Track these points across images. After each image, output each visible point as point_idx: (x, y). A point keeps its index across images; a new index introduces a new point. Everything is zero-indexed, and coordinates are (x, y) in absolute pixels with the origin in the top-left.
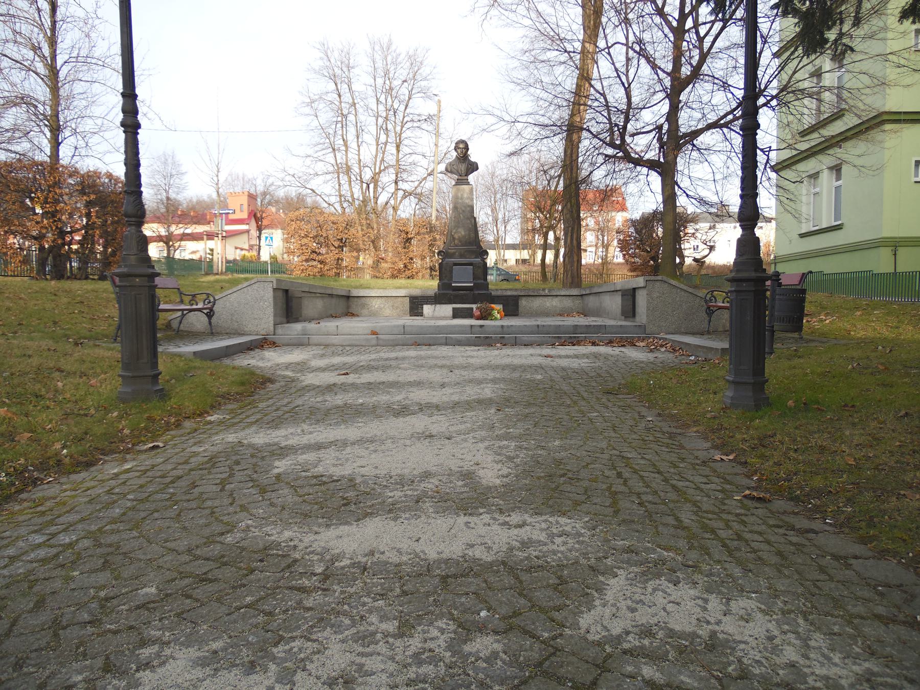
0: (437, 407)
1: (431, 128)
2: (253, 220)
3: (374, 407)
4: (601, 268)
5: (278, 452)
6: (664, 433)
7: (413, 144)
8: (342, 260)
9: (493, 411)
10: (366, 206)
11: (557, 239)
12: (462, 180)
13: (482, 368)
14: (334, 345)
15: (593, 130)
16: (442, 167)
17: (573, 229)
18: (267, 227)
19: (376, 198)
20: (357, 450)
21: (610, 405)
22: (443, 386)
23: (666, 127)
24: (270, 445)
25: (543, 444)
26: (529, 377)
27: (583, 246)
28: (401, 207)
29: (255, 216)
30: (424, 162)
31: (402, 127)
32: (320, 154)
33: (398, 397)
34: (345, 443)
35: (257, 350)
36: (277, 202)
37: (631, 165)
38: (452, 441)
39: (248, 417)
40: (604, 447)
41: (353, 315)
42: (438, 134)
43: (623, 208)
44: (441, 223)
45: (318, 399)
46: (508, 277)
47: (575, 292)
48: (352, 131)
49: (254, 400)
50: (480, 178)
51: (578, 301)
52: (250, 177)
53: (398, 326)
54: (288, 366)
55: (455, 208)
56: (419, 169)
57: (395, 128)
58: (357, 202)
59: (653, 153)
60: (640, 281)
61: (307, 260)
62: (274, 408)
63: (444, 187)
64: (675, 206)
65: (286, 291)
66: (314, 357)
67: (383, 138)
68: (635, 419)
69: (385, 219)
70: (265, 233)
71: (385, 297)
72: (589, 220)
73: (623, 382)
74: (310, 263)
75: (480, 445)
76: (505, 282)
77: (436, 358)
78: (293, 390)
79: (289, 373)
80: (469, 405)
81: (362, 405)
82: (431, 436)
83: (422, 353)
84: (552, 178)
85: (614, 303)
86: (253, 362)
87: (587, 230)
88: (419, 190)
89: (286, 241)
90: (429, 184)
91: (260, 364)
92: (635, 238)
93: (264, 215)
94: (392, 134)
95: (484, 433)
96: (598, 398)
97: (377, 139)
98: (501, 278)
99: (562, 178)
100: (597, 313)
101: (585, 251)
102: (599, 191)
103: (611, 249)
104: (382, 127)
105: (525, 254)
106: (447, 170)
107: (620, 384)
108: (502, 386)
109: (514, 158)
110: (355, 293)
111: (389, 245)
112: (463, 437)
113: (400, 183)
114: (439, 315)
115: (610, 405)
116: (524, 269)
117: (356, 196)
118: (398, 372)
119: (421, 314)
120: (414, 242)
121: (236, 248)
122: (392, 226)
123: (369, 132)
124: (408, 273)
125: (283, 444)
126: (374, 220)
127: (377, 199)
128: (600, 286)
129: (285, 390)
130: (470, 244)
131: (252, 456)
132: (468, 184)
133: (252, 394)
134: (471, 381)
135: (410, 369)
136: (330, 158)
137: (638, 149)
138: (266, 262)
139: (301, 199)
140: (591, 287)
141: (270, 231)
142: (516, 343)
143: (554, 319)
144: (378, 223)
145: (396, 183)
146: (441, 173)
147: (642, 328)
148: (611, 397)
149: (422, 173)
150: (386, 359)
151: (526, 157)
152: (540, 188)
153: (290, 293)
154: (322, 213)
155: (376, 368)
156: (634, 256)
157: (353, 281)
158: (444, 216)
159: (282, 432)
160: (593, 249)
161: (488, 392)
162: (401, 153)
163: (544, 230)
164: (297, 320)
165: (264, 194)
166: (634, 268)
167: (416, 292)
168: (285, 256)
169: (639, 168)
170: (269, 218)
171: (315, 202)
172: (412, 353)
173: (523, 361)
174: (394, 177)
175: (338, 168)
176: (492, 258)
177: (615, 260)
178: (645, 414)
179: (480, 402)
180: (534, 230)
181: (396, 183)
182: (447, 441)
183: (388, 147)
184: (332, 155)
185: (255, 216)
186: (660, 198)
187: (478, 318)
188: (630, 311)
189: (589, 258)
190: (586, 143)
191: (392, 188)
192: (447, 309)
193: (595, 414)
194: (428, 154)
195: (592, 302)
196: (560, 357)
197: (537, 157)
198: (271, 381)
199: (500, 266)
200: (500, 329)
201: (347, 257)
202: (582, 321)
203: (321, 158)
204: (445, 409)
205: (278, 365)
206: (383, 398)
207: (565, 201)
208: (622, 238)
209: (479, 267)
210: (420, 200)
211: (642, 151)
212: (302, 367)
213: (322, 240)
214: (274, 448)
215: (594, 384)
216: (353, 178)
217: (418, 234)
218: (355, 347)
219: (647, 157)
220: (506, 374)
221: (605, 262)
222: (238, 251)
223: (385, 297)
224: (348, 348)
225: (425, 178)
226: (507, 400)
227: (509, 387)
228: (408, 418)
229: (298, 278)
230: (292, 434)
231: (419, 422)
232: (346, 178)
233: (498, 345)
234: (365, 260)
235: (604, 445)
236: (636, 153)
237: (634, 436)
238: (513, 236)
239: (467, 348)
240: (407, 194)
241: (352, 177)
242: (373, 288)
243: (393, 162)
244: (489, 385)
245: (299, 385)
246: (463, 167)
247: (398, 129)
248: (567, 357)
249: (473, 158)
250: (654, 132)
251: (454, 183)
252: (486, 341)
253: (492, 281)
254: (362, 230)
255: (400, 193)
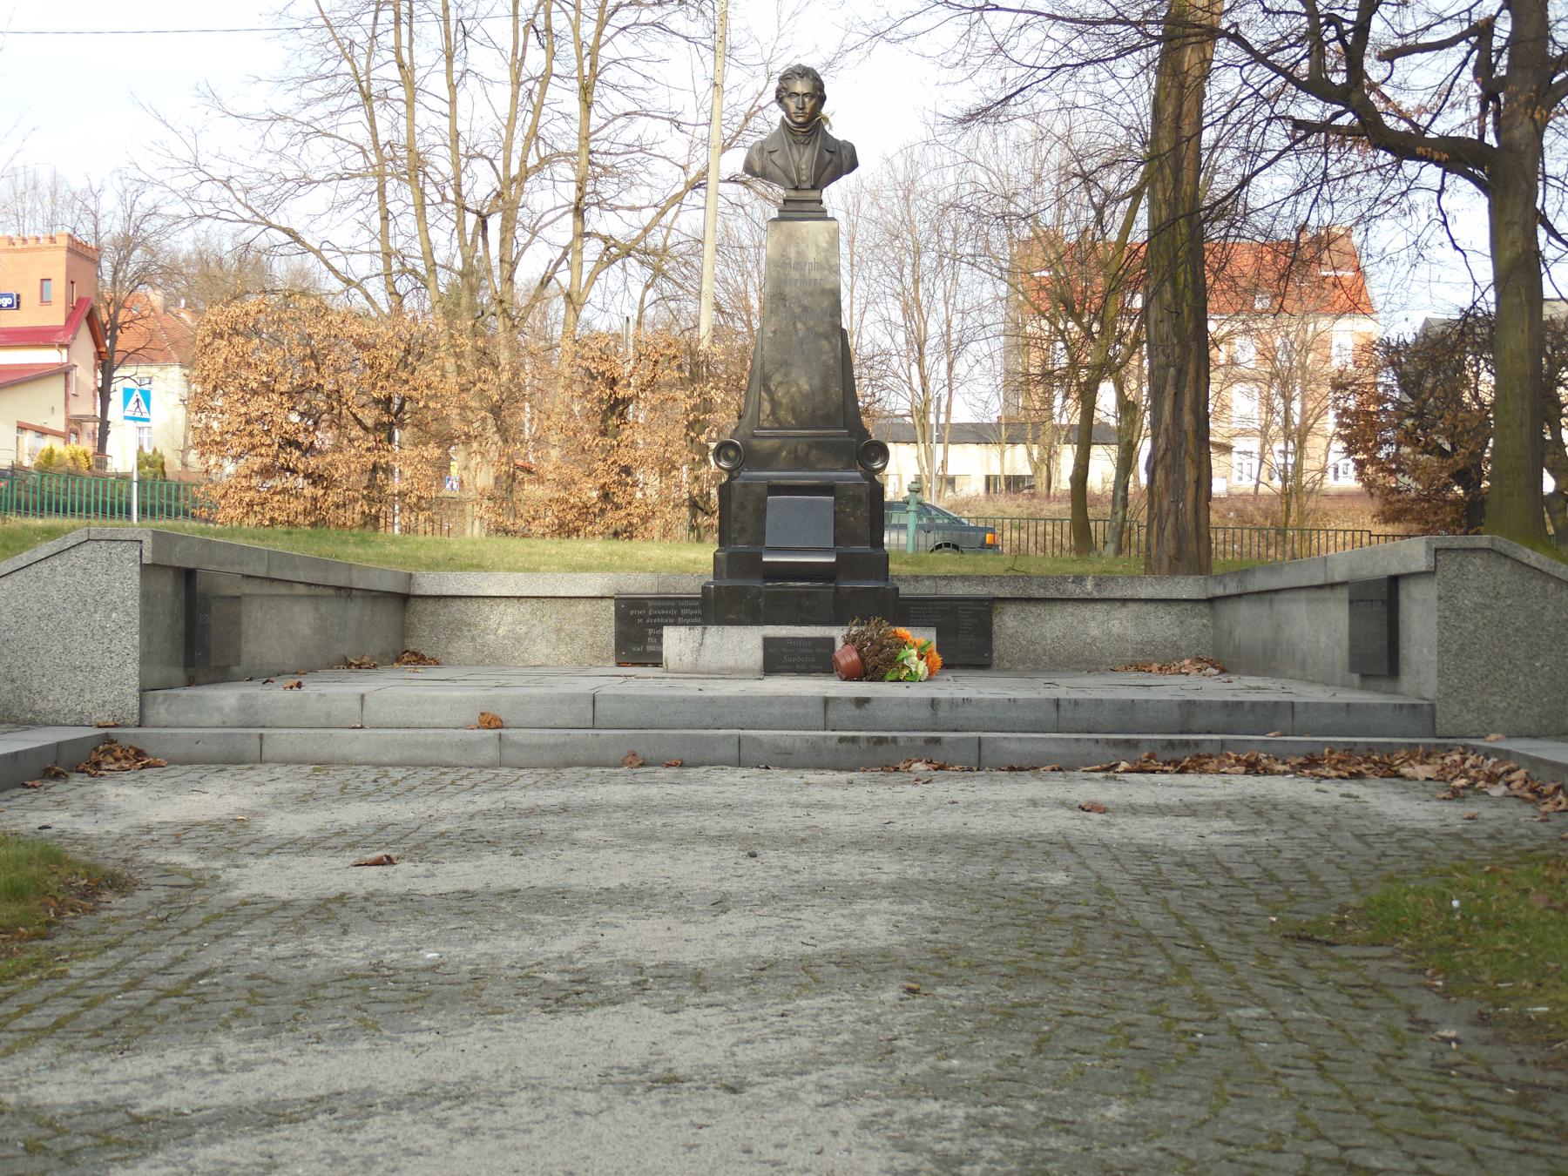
0: (698, 980)
1: (698, 29)
2: (84, 333)
3: (477, 977)
4: (1278, 507)
5: (124, 1135)
6: (1498, 1085)
7: (637, 81)
8: (388, 470)
9: (891, 994)
10: (473, 290)
11: (1126, 407)
12: (801, 203)
13: (861, 844)
14: (348, 763)
15: (1251, 36)
16: (734, 161)
17: (1181, 372)
18: (131, 356)
19: (510, 264)
20: (406, 1127)
21: (1307, 979)
22: (721, 904)
23: (1504, 27)
24: (96, 1109)
25: (1066, 1114)
26: (1021, 876)
27: (1217, 431)
28: (595, 294)
29: (91, 318)
30: (676, 145)
31: (602, 24)
32: (319, 110)
33: (564, 942)
34: (364, 1104)
35: (77, 778)
36: (171, 272)
37: (1384, 158)
38: (746, 1098)
39: (26, 1010)
40: (1285, 1128)
41: (420, 659)
42: (721, 48)
43: (1357, 304)
44: (729, 351)
45: (280, 950)
46: (957, 536)
47: (1187, 587)
48: (429, 36)
49: (54, 953)
50: (866, 199)
51: (1198, 622)
52: (79, 184)
53: (573, 699)
54: (181, 835)
55: (777, 298)
56: (659, 166)
57: (576, 29)
58: (443, 277)
59: (1460, 116)
60: (1414, 553)
61: (266, 472)
62: (124, 978)
63: (742, 230)
64: (1537, 298)
65: (188, 576)
66: (277, 802)
67: (535, 60)
68: (1395, 1034)
69: (539, 335)
70: (124, 379)
71: (534, 597)
72: (1237, 345)
73: (1354, 900)
74: (276, 482)
75: (843, 1112)
76: (947, 554)
77: (700, 807)
78: (196, 917)
79: (185, 859)
80: (808, 974)
81: (433, 968)
82: (671, 1080)
83: (654, 792)
84: (1110, 198)
85: (1324, 629)
86: (60, 820)
87: (1230, 380)
88: (656, 239)
89: (197, 404)
90: (689, 220)
91: (86, 826)
92: (1399, 405)
93: (122, 316)
94: (567, 49)
95: (856, 1072)
96: (1263, 957)
97: (517, 64)
98: (934, 538)
99: (1144, 202)
100: (1264, 661)
101: (1226, 449)
102: (1277, 247)
103: (1315, 445)
104: (531, 24)
105: (1018, 460)
106: (748, 168)
107: (1343, 909)
108: (927, 908)
109: (982, 133)
110: (428, 583)
111: (553, 418)
112: (783, 1083)
113: (592, 214)
114: (716, 660)
115: (1307, 979)
116: (1013, 510)
117: (440, 256)
118: (569, 855)
119: (655, 660)
120: (638, 413)
121: (22, 428)
122: (562, 362)
123: (489, 42)
124: (615, 518)
125: (144, 1107)
126: (502, 338)
127: (513, 265)
128: (1274, 568)
129: (164, 919)
130: (827, 421)
131: (31, 1149)
132: (822, 215)
133: (47, 930)
134: (819, 890)
135: (607, 845)
136: (354, 126)
137: (1408, 102)
138: (125, 477)
139: (251, 263)
140: (1244, 573)
141: (143, 371)
142: (978, 762)
143: (1114, 679)
144: (516, 350)
145: (579, 211)
146: (733, 180)
147: (1423, 714)
148: (1310, 952)
149: (669, 179)
150: (530, 812)
151: (1022, 130)
152: (1071, 235)
153: (201, 584)
154: (321, 311)
155: (491, 843)
156: (1395, 466)
157: (427, 543)
158: (739, 325)
159: (145, 1064)
160: (1254, 444)
161: (876, 927)
162: (597, 110)
163: (1084, 375)
164: (222, 675)
165: (127, 244)
166: (1395, 510)
167: (640, 584)
168: (193, 457)
169: (1410, 167)
170: (140, 328)
171: (303, 274)
172: (620, 790)
173: (1005, 824)
174: (569, 193)
175: (382, 162)
176: (901, 470)
177: (1330, 484)
178: (1433, 1016)
179: (849, 962)
180: (1047, 375)
181: (579, 211)
182: (726, 1099)
183: (552, 92)
184: (360, 115)
185: (91, 318)
186: (1485, 271)
187: (852, 675)
188: (1379, 654)
189: (1235, 475)
190: (1226, 82)
191: (564, 231)
192: (743, 643)
193: (1254, 1012)
194: (689, 116)
195: (1247, 622)
196: (1133, 810)
197: (1059, 129)
198: (119, 884)
199: (929, 499)
200: (925, 713)
201: (407, 460)
202: (1212, 688)
203: (325, 124)
204: (724, 984)
205: (149, 830)
206: (510, 946)
207: (1156, 279)
208: (1352, 404)
209: (857, 500)
210: (659, 272)
211: (1421, 109)
212: (233, 838)
213: (320, 402)
214: (113, 1119)
215: (1252, 907)
216: (432, 193)
217: (652, 385)
218: (432, 767)
219: (1440, 128)
220: (944, 867)
221: (1294, 490)
222: (29, 438)
223: (534, 597)
224: (397, 774)
225: (677, 199)
226: (943, 957)
227: (952, 912)
228: (592, 1018)
229: (232, 533)
230: (178, 1070)
231: (631, 1033)
232: (407, 193)
233: (919, 767)
234: (471, 472)
235: (1283, 1119)
236: (1402, 115)
237: (1393, 1094)
238: (977, 396)
239: (811, 776)
240: (615, 252)
241: (430, 189)
242: (493, 568)
243: (569, 143)
244: (884, 905)
245: (218, 900)
246: (804, 159)
247: (588, 29)
248: (1158, 810)
249: (838, 129)
250: (1463, 46)
251: (775, 214)
252: (876, 753)
253: (901, 551)
254: (460, 370)
255: (593, 248)
